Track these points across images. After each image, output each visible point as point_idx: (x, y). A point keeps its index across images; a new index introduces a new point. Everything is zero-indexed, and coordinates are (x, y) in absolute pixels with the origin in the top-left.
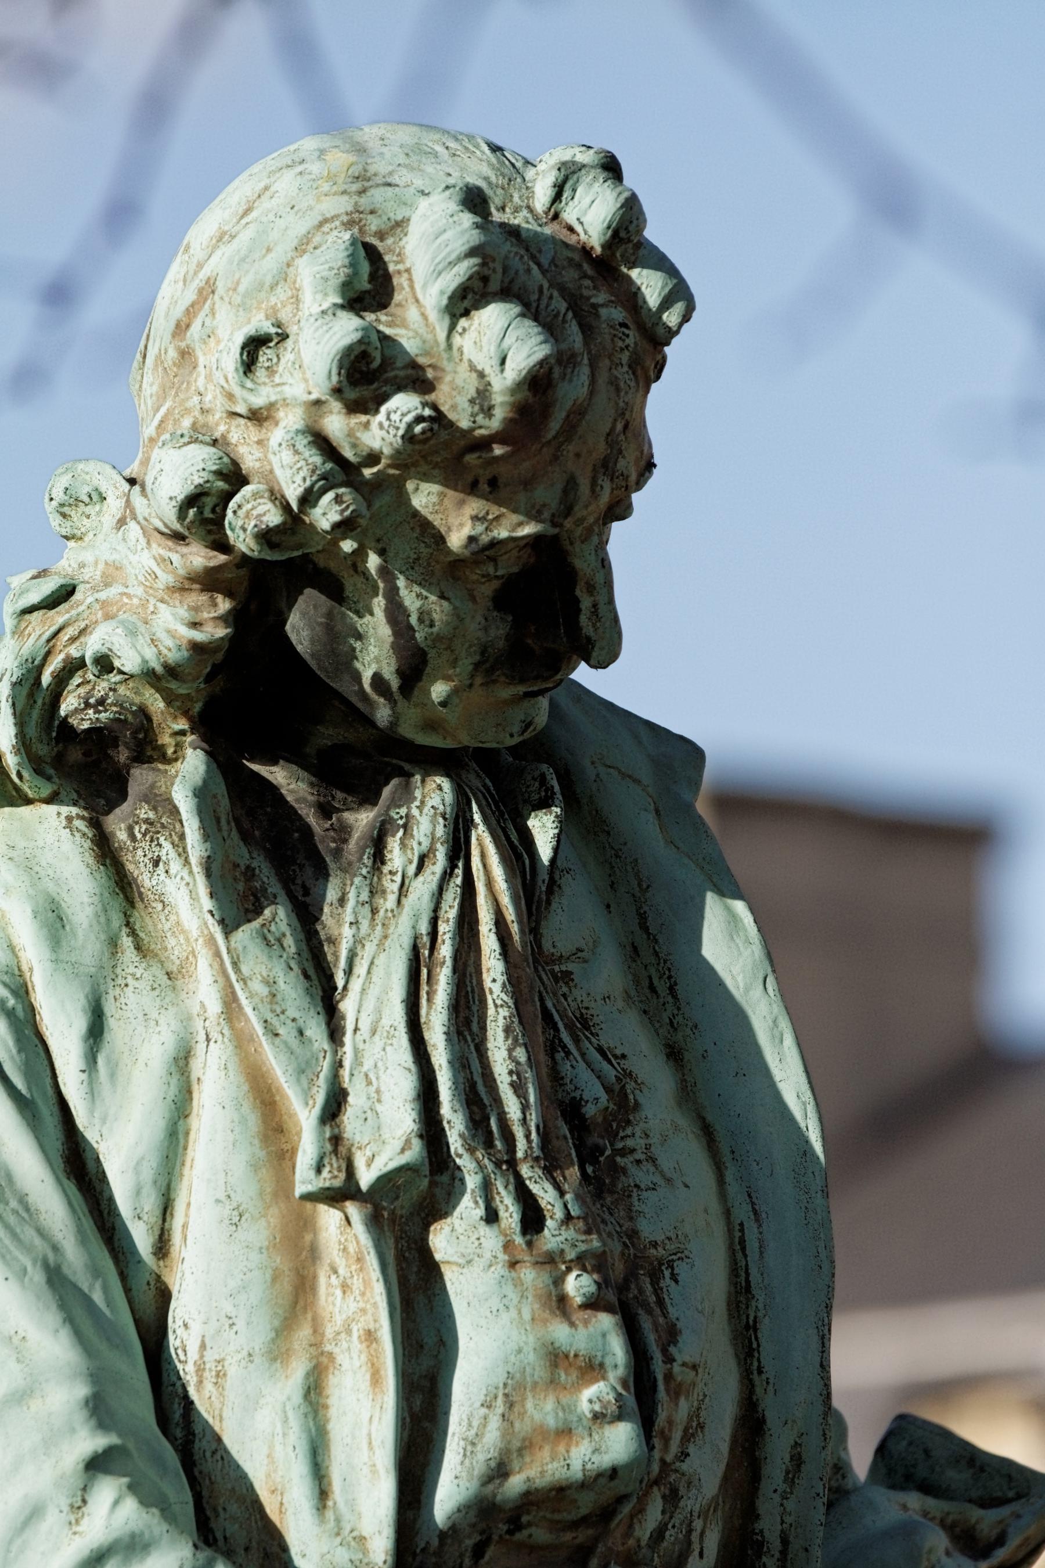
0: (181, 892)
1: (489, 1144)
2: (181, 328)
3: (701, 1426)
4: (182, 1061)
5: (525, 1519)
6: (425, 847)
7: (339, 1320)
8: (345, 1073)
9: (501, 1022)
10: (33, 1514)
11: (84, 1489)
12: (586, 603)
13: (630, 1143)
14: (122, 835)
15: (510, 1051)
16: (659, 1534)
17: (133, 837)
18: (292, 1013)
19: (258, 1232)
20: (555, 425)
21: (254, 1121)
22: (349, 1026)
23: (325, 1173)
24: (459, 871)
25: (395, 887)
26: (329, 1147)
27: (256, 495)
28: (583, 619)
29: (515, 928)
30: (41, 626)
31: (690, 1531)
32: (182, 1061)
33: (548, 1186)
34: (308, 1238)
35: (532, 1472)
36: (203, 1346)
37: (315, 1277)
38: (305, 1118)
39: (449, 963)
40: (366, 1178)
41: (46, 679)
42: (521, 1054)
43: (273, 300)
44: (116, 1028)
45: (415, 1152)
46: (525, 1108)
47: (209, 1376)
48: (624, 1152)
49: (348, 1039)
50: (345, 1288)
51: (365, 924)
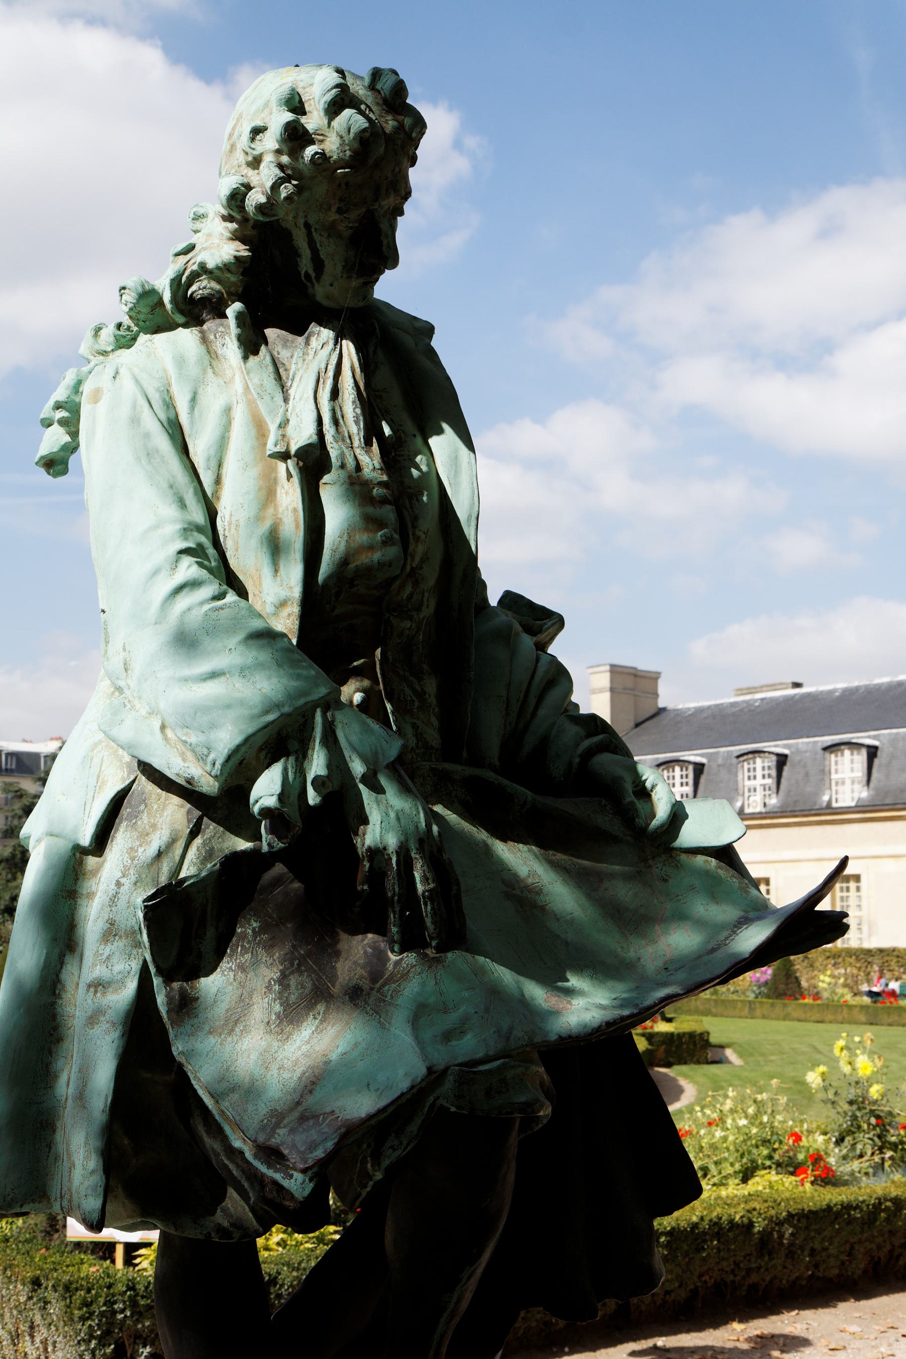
0: (231, 349)
1: (343, 440)
2: (231, 136)
3: (428, 559)
4: (228, 411)
5: (356, 582)
6: (325, 340)
7: (284, 505)
8: (289, 413)
9: (351, 400)
10: (156, 572)
11: (176, 562)
12: (385, 242)
13: (402, 453)
14: (212, 337)
15: (354, 409)
16: (410, 597)
17: (216, 338)
18: (269, 391)
19: (254, 472)
20: (371, 161)
21: (253, 432)
22: (291, 398)
23: (278, 447)
24: (338, 347)
25: (313, 353)
26: (280, 438)
27: (256, 192)
28: (384, 249)
29: (364, 393)
30: (183, 259)
31: (423, 596)
32: (228, 411)
33: (367, 457)
34: (273, 475)
35: (358, 563)
36: (231, 515)
37: (276, 490)
38: (273, 427)
39: (332, 378)
40: (293, 449)
41: (184, 279)
42: (359, 411)
43: (263, 115)
44: (202, 399)
45: (314, 439)
46: (359, 430)
47: (233, 526)
48: (399, 456)
49: (291, 402)
50: (287, 493)
51: (300, 364)
